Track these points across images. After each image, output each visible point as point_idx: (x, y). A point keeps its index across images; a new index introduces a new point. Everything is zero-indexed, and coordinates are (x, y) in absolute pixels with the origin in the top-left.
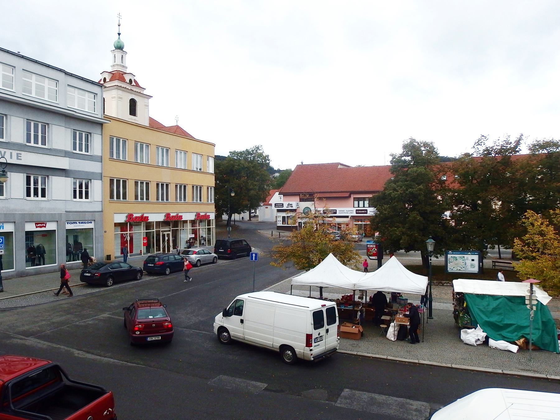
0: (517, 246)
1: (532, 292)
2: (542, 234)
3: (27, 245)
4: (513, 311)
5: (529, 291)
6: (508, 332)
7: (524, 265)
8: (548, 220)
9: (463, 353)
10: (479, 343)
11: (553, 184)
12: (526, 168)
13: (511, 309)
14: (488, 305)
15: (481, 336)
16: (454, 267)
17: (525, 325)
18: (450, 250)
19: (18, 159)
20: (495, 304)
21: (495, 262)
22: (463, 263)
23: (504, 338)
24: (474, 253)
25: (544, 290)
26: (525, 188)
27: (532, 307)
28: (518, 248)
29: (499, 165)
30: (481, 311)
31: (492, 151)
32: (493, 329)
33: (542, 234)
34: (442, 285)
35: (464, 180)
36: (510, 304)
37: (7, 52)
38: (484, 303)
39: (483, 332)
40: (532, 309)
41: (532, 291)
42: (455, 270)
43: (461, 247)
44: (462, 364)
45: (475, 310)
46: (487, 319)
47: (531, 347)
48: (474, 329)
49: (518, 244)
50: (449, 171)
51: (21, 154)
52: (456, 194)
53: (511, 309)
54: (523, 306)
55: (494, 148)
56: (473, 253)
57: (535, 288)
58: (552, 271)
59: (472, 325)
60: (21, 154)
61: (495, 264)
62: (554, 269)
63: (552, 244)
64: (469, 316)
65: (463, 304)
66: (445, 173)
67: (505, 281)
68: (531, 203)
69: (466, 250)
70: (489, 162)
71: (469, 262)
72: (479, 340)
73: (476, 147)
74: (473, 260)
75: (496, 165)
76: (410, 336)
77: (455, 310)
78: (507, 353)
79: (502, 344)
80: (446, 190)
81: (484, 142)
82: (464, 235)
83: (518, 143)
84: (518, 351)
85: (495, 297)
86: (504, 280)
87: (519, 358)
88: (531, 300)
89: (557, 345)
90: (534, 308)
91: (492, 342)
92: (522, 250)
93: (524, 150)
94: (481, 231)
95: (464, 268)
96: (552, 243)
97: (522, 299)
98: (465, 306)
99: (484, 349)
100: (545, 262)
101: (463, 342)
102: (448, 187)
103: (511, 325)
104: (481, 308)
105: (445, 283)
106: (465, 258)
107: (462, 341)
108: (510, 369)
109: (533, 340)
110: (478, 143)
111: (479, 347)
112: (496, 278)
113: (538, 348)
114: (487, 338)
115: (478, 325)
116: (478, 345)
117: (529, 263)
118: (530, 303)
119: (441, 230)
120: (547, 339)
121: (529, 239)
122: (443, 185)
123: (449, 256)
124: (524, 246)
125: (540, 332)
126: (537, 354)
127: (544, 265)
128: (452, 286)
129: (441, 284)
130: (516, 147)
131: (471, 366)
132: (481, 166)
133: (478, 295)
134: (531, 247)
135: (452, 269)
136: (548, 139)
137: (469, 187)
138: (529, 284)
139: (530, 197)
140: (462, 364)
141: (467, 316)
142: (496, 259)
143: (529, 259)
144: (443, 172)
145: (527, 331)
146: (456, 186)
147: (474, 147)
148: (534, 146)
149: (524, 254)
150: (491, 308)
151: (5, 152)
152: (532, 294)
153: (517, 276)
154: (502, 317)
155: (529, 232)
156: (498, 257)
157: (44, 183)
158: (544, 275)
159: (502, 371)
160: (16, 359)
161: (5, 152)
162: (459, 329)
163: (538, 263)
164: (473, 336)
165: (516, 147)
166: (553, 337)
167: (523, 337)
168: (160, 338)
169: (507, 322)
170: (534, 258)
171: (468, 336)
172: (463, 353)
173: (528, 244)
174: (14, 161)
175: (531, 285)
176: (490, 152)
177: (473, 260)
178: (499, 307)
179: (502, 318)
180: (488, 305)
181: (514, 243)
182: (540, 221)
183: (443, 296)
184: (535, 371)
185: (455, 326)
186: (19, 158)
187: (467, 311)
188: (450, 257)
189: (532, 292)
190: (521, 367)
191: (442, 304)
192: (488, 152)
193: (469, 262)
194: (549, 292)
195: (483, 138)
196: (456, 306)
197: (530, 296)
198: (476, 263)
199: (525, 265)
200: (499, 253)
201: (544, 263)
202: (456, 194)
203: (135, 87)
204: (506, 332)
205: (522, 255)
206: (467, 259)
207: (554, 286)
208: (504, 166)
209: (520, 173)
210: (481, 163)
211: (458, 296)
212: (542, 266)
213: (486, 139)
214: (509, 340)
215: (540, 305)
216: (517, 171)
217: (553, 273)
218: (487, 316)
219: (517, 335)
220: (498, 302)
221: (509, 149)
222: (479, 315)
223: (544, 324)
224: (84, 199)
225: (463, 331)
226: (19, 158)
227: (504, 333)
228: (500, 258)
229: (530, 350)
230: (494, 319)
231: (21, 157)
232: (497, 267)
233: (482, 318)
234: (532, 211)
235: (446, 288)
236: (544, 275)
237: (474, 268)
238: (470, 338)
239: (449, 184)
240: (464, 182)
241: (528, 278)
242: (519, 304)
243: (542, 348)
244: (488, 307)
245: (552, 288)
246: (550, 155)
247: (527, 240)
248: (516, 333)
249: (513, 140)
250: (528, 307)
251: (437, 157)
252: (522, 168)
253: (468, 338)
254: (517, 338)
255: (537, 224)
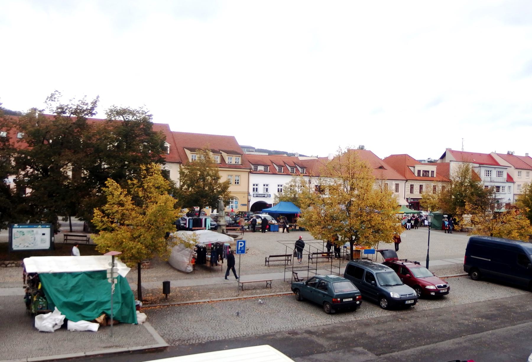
0: (97, 217)
1: (113, 265)
2: (121, 204)
3: (115, 255)
4: (93, 286)
5: (111, 264)
6: (88, 311)
7: (103, 237)
8: (126, 190)
9: (39, 342)
10: (57, 328)
11: (128, 153)
12: (103, 133)
13: (91, 285)
14: (66, 284)
15: (59, 319)
16: (20, 244)
18: (16, 223)
20: (73, 282)
21: (67, 235)
22: (32, 238)
23: (84, 318)
24: (45, 226)
25: (123, 262)
26: (100, 154)
27: (114, 280)
28: (97, 219)
29: (74, 126)
30: (58, 291)
31: (66, 109)
32: (72, 310)
33: (121, 204)
34: (5, 266)
35: (33, 139)
36: (90, 279)
38: (62, 282)
39: (61, 314)
40: (113, 282)
41: (114, 264)
42: (21, 247)
43: (29, 219)
44: (40, 355)
45: (51, 291)
46: (65, 300)
47: (112, 322)
48: (50, 313)
49: (98, 215)
50: (15, 127)
52: (23, 156)
53: (91, 285)
54: (103, 281)
55: (69, 107)
56: (43, 225)
57: (117, 262)
58: (130, 242)
59: (49, 308)
61: (67, 238)
62: (131, 239)
63: (131, 214)
64: (45, 298)
65: (37, 287)
66: (9, 128)
67: (81, 255)
68: (106, 171)
69: (34, 223)
70: (63, 122)
71: (39, 237)
72: (56, 324)
73: (48, 102)
74: (44, 234)
75: (71, 126)
77: (28, 295)
78: (87, 333)
79: (82, 325)
80: (9, 149)
81: (58, 98)
82: (32, 206)
83: (95, 103)
84: (99, 329)
85: (73, 275)
86: (79, 254)
87: (101, 337)
88: (112, 273)
89: (135, 316)
90: (116, 281)
91: (71, 325)
92: (102, 221)
93: (100, 114)
94: (53, 200)
95: (32, 243)
96: (130, 214)
97: (102, 274)
98: (39, 287)
99: (64, 333)
100: (124, 233)
101: (38, 330)
102: (13, 146)
103: (91, 302)
104: (59, 288)
105: (9, 263)
106: (35, 232)
107: (36, 330)
108: (92, 350)
109: (113, 315)
110: (52, 97)
111: (58, 333)
112: (69, 253)
113: (118, 323)
114: (66, 321)
116: (56, 331)
117: (108, 235)
118: (112, 277)
119: (5, 199)
120: (126, 312)
121: (109, 210)
122: (7, 144)
123: (14, 230)
124: (104, 217)
125: (120, 304)
126: (117, 328)
127: (123, 236)
128: (23, 266)
129: (3, 265)
130: (92, 109)
131: (50, 355)
132: (55, 126)
133: (55, 274)
134: (110, 218)
135: (18, 246)
136: (124, 106)
137: (40, 148)
138: (111, 257)
139: (104, 164)
140: (40, 355)
141: (42, 299)
142: (67, 231)
143: (108, 230)
144: (7, 127)
145: (108, 306)
146: (24, 146)
147: (46, 102)
148: (111, 111)
149: (104, 225)
150: (70, 285)
152: (113, 266)
153: (96, 249)
154: (82, 295)
155: (109, 202)
156: (69, 230)
158: (123, 246)
159: (85, 353)
162: (32, 316)
163: (117, 234)
164: (50, 321)
165: (92, 109)
166: (132, 308)
167: (103, 313)
169: (86, 300)
170: (112, 230)
171: (44, 322)
172: (39, 342)
173: (108, 215)
175: (113, 257)
176: (64, 110)
177: (44, 234)
178: (78, 284)
179: (82, 296)
180: (66, 284)
181: (94, 213)
182: (120, 190)
183: (8, 279)
184: (117, 346)
185: (26, 313)
187: (42, 293)
188: (16, 231)
189: (113, 265)
190: (104, 345)
191: (7, 289)
192: (62, 110)
193: (39, 237)
194: (127, 263)
195: (56, 93)
196: (28, 289)
197: (112, 269)
198: (47, 237)
199: (104, 236)
200: (71, 225)
201: (123, 234)
202: (23, 156)
204: (86, 311)
205: (102, 226)
206: (37, 233)
207: (132, 256)
208: (80, 128)
209: (97, 138)
210: (53, 122)
211: (31, 278)
212: (121, 237)
213: (60, 96)
214: (89, 319)
215: (121, 279)
216: (94, 135)
217: (131, 244)
218: (65, 296)
219: (97, 312)
220: (77, 279)
221: (84, 111)
222: (56, 296)
223: (124, 296)
225: (37, 318)
227: (84, 312)
228: (71, 231)
229: (112, 325)
230: (73, 298)
232: (68, 242)
233: (59, 299)
234: (112, 180)
235: (10, 269)
236: (123, 246)
237: (44, 243)
238: (47, 324)
239: (14, 143)
240: (33, 142)
241: (107, 251)
242: (100, 278)
243: (122, 321)
244: (67, 286)
245: (130, 259)
246: (126, 123)
247: (107, 210)
248: (96, 310)
249: (89, 101)
250: (110, 281)
251: (24, 117)
252: (98, 133)
253: (45, 325)
254: (98, 315)
255: (117, 193)
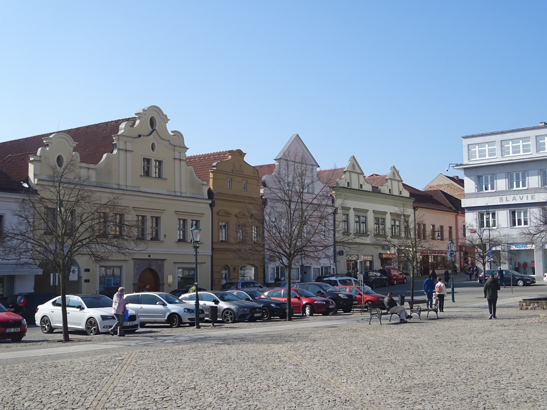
17: (275, 288)
19: (532, 199)
37: (534, 128)
51: (534, 195)
60: (534, 195)
76: (479, 281)
115: (430, 274)
151: (523, 196)
157: (525, 215)
160: (117, 345)
161: (523, 196)
168: (19, 331)
174: (530, 201)
186: (533, 198)
203: (372, 193)
222: (14, 316)
224: (523, 225)
226: (533, 198)
231: (534, 197)
